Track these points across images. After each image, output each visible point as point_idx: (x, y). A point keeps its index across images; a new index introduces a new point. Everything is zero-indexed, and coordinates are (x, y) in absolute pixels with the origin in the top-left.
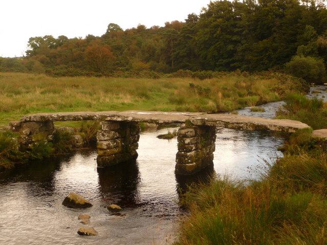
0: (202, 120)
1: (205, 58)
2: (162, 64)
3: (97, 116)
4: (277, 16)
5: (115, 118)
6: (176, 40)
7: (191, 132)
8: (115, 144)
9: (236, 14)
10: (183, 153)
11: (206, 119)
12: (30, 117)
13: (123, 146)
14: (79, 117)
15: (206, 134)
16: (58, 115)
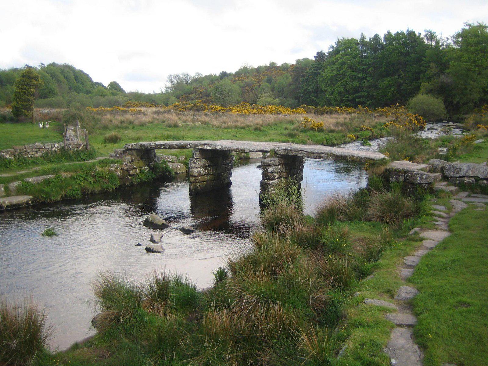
0: (286, 149)
1: (331, 94)
2: (292, 101)
3: (190, 144)
4: (402, 54)
5: (205, 147)
6: (304, 76)
7: (274, 161)
8: (206, 171)
9: (362, 51)
10: (266, 181)
11: (289, 148)
12: (132, 146)
13: (214, 174)
14: (174, 145)
15: (292, 165)
16: (155, 144)
